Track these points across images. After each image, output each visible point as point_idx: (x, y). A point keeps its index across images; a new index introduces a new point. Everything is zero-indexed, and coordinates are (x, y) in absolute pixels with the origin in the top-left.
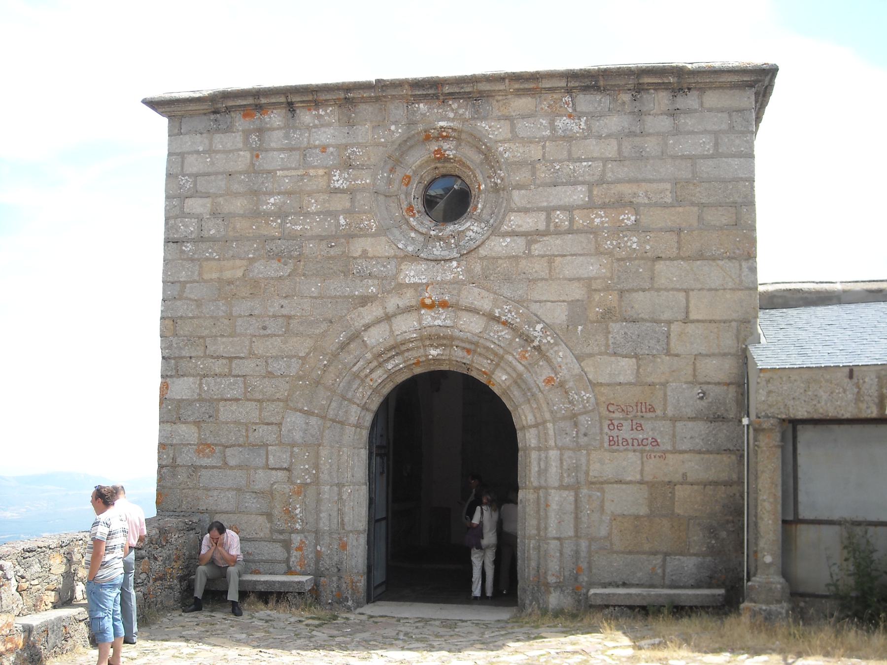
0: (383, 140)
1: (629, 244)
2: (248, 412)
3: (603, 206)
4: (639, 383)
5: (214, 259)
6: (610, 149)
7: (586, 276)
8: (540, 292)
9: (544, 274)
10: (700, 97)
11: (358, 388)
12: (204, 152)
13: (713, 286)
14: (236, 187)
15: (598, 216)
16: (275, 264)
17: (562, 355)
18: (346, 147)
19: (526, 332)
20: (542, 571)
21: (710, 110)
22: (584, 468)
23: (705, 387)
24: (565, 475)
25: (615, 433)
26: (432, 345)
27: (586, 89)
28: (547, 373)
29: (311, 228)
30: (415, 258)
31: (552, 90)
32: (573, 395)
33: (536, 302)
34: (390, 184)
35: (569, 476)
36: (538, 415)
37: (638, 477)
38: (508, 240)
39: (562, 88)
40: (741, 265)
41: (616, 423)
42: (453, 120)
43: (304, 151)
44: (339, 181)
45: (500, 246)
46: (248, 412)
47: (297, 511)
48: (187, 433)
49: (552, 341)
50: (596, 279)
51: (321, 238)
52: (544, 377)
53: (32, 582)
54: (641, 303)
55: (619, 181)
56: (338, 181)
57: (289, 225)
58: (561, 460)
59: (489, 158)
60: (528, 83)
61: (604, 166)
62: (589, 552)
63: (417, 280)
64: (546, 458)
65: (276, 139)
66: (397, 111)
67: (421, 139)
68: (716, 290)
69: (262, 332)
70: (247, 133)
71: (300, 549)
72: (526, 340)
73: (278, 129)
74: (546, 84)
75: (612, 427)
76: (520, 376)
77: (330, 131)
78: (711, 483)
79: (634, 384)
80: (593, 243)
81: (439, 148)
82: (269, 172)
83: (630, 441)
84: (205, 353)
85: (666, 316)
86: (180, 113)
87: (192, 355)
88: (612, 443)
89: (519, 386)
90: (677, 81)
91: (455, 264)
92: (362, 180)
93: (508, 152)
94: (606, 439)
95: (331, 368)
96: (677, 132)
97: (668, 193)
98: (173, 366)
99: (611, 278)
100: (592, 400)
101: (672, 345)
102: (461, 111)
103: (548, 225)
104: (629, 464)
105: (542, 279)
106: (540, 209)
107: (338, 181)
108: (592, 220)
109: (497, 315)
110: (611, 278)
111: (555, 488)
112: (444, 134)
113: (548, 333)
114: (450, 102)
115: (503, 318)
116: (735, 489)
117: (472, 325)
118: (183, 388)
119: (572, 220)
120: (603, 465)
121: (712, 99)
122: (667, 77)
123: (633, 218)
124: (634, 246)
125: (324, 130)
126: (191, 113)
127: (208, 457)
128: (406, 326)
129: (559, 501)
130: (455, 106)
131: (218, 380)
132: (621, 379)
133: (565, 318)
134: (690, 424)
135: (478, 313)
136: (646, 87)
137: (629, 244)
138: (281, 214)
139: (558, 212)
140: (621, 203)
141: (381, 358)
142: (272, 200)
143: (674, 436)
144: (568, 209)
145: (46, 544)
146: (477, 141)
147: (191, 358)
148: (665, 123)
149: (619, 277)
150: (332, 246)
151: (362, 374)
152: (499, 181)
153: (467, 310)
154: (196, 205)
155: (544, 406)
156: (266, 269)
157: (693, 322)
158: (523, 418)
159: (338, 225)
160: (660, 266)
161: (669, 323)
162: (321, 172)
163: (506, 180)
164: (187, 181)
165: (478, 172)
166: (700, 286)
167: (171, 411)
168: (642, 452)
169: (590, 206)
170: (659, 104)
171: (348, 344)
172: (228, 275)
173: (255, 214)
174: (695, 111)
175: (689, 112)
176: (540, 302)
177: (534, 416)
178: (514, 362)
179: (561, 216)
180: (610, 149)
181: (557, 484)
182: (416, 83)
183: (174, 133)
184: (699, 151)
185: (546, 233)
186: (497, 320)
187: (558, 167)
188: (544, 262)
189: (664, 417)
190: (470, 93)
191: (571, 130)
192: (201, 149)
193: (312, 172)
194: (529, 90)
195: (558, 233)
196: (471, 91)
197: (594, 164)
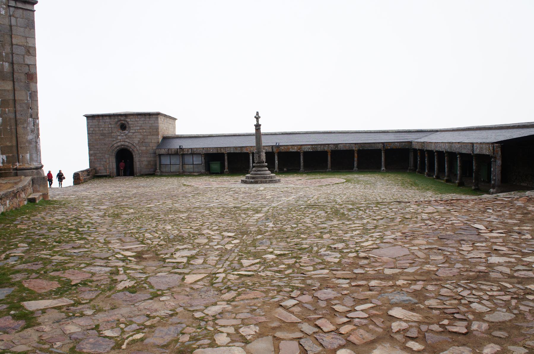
2: (100, 155)
6: (142, 122)
8: (135, 139)
17: (137, 147)
43: (105, 122)
44: (110, 126)
45: (130, 134)
46: (100, 155)
48: (92, 158)
54: (146, 141)
59: (128, 123)
65: (101, 121)
66: (116, 117)
81: (122, 121)
90: (150, 115)
93: (130, 123)
98: (90, 150)
104: (145, 159)
117: (127, 144)
118: (92, 152)
120: (143, 159)
121: (154, 116)
128: (119, 144)
129: (138, 163)
138: (103, 130)
140: (143, 129)
141: (116, 148)
146: (126, 121)
148: (148, 119)
154: (91, 129)
156: (101, 137)
167: (90, 155)
173: (99, 130)
180: (142, 122)
183: (87, 120)
196: (126, 115)
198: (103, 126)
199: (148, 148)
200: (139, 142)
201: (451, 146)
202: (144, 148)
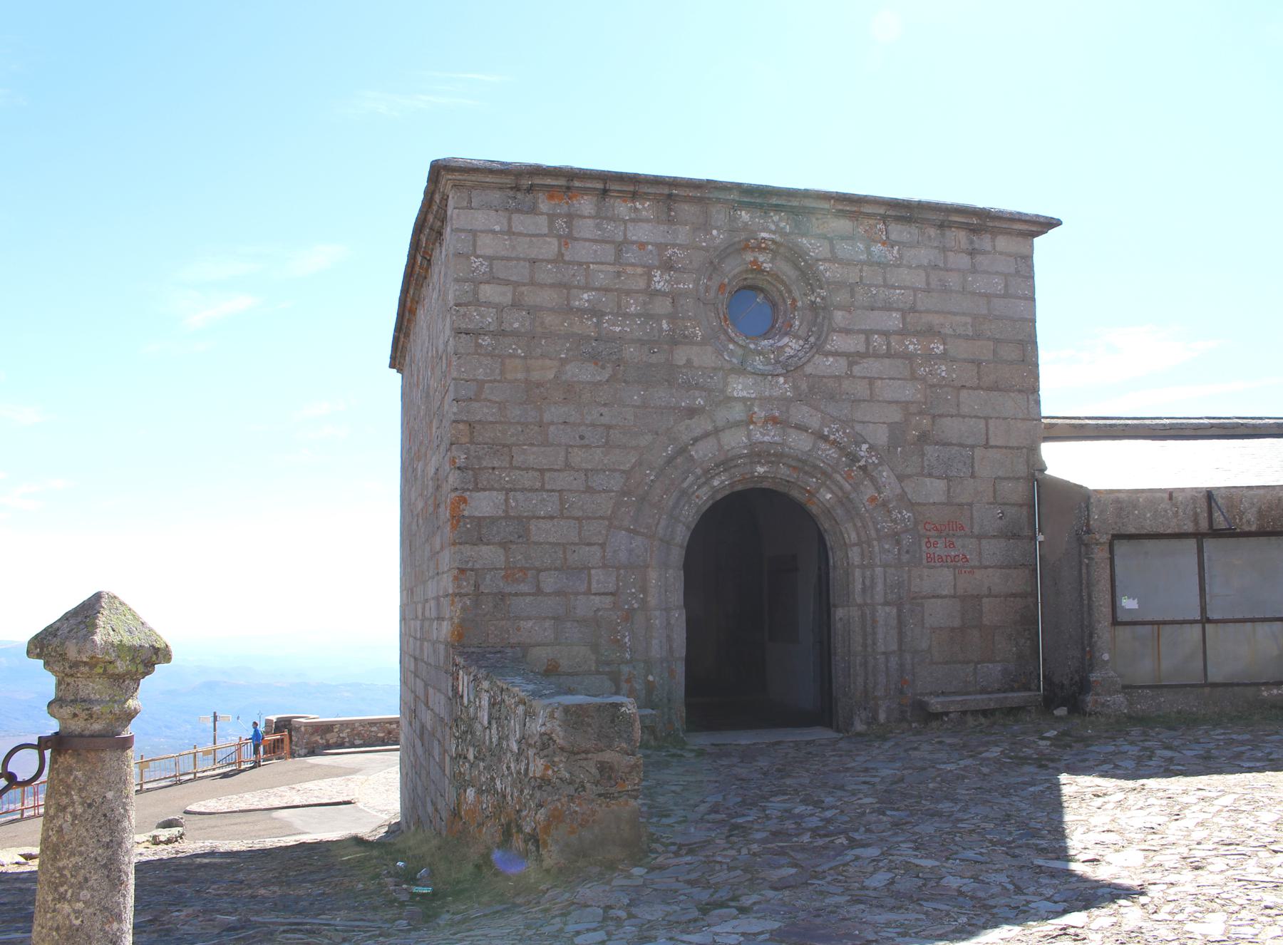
3: (917, 333)
10: (993, 240)
12: (501, 232)
25: (932, 550)
26: (759, 462)
28: (870, 492)
31: (869, 215)
32: (895, 514)
38: (831, 359)
41: (932, 540)
42: (774, 233)
44: (660, 281)
51: (641, 342)
55: (928, 311)
63: (745, 394)
65: (586, 228)
70: (552, 218)
85: (970, 441)
89: (843, 504)
91: (781, 380)
96: (974, 270)
99: (925, 403)
103: (867, 348)
110: (925, 403)
115: (832, 437)
119: (889, 345)
130: (776, 218)
133: (886, 439)
142: (585, 296)
144: (885, 334)
148: (965, 261)
156: (582, 373)
157: (992, 447)
159: (661, 330)
160: (964, 393)
161: (972, 447)
162: (639, 270)
165: (794, 288)
168: (955, 568)
169: (904, 333)
172: (536, 376)
174: (989, 253)
175: (984, 253)
177: (858, 534)
178: (842, 482)
185: (865, 355)
186: (825, 438)
192: (497, 228)
193: (629, 270)
195: (876, 355)
198: (602, 277)
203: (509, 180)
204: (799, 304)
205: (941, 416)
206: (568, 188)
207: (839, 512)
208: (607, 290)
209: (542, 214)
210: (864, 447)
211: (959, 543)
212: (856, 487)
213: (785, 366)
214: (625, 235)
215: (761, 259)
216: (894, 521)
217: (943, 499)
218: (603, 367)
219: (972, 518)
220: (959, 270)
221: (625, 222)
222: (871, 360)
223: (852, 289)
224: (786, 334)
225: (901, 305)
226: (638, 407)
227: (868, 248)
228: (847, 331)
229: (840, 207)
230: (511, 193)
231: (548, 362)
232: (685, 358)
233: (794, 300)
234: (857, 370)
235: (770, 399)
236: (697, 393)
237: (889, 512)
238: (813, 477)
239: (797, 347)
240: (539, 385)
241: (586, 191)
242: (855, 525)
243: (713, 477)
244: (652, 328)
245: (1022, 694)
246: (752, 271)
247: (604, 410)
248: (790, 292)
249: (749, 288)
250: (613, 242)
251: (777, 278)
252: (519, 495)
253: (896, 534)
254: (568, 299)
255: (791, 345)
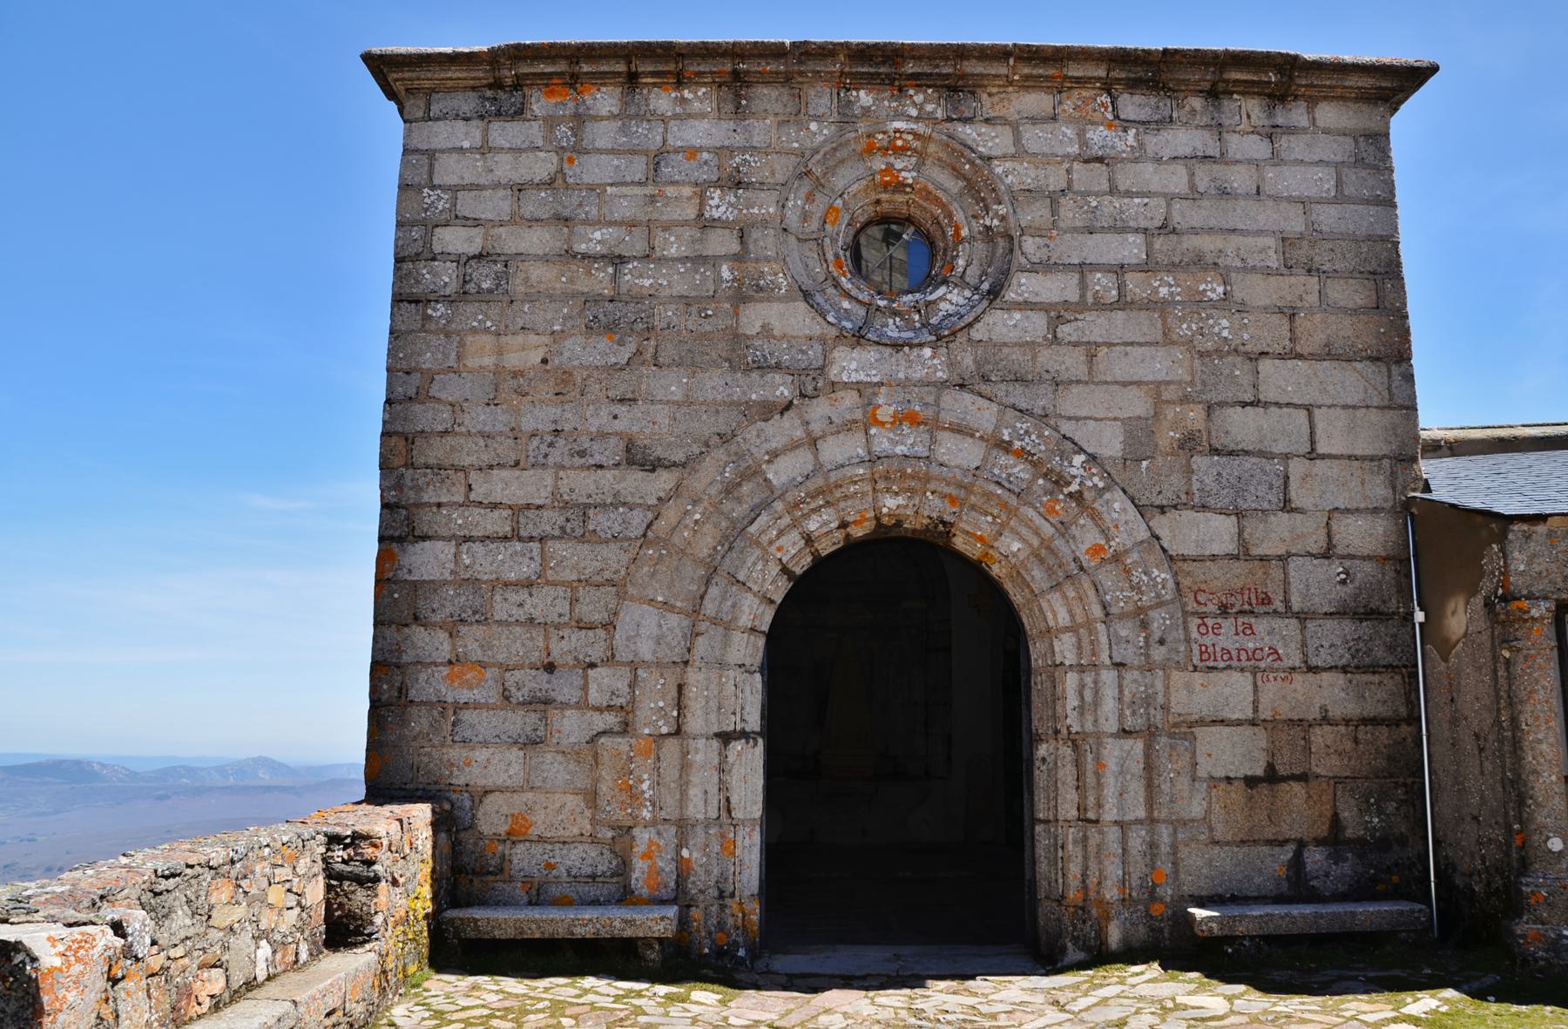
0: (796, 145)
1: (1216, 329)
3: (1173, 267)
4: (1243, 553)
5: (487, 330)
7: (1151, 378)
8: (1073, 402)
9: (1081, 371)
10: (1310, 110)
11: (755, 564)
12: (471, 150)
13: (1349, 402)
14: (529, 209)
15: (1163, 283)
16: (603, 343)
18: (731, 150)
19: (1058, 469)
20: (1093, 880)
21: (1327, 131)
22: (1160, 699)
23: (1347, 563)
24: (1128, 712)
25: (1208, 640)
26: (888, 490)
27: (1133, 85)
28: (1091, 537)
29: (670, 285)
30: (858, 338)
31: (1081, 82)
32: (1138, 575)
33: (1069, 418)
34: (805, 220)
35: (1134, 713)
36: (1078, 611)
37: (1250, 714)
38: (1017, 316)
39: (1099, 79)
40: (1389, 371)
41: (1210, 622)
42: (917, 119)
44: (719, 205)
47: (645, 786)
49: (1101, 485)
50: (1168, 383)
51: (686, 301)
52: (1087, 546)
53: (173, 953)
55: (1194, 231)
56: (718, 207)
57: (628, 277)
58: (1120, 686)
59: (979, 186)
60: (1046, 65)
61: (1169, 205)
62: (1174, 848)
63: (862, 377)
64: (1096, 682)
65: (603, 134)
67: (859, 149)
68: (1354, 407)
69: (578, 461)
70: (551, 122)
71: (647, 856)
72: (1056, 482)
73: (608, 118)
74: (1075, 70)
75: (1203, 630)
76: (1047, 544)
77: (704, 125)
78: (1365, 721)
79: (1237, 558)
80: (1159, 326)
82: (591, 188)
83: (1234, 654)
84: (467, 497)
85: (1280, 448)
86: (427, 84)
87: (444, 500)
88: (1205, 656)
89: (1042, 561)
90: (1282, 79)
91: (927, 352)
92: (761, 207)
93: (1011, 174)
94: (1196, 648)
95: (708, 527)
96: (1276, 159)
97: (1271, 253)
99: (1192, 383)
100: (1171, 584)
101: (1293, 495)
102: (929, 108)
103: (1083, 296)
105: (1078, 382)
106: (1068, 267)
107: (718, 207)
108: (1156, 291)
109: (1006, 438)
110: (1192, 383)
111: (1112, 735)
112: (899, 143)
113: (1094, 471)
114: (911, 92)
115: (1017, 444)
116: (1405, 729)
119: (1121, 288)
120: (1193, 694)
122: (1266, 73)
123: (1220, 289)
124: (1225, 333)
125: (695, 122)
126: (450, 83)
127: (471, 688)
130: (919, 98)
131: (492, 546)
132: (1217, 549)
133: (1119, 447)
134: (1330, 624)
135: (972, 436)
136: (1230, 87)
137: (1216, 329)
139: (1099, 275)
140: (1199, 263)
142: (598, 235)
143: (1304, 644)
144: (1120, 269)
145: (203, 860)
146: (960, 158)
147: (439, 505)
148: (1257, 147)
149: (1204, 383)
150: (707, 316)
151: (764, 539)
152: (996, 222)
153: (953, 430)
155: (1091, 593)
156: (584, 352)
157: (1323, 457)
158: (1049, 615)
159: (718, 279)
160: (1266, 365)
161: (1286, 457)
162: (687, 191)
163: (1011, 219)
164: (439, 198)
165: (954, 207)
166: (1330, 402)
168: (1255, 671)
169: (1148, 267)
170: (1249, 117)
171: (740, 484)
172: (513, 360)
174: (1304, 130)
175: (1291, 130)
176: (1077, 419)
177: (1070, 612)
178: (1039, 521)
179: (1104, 281)
180: (1177, 180)
181: (1114, 729)
182: (862, 51)
184: (1313, 192)
185: (1081, 306)
186: (1006, 447)
187: (1094, 204)
188: (1079, 355)
189: (1288, 612)
190: (947, 76)
191: (1113, 147)
192: (466, 145)
193: (670, 191)
194: (1047, 78)
195: (1100, 306)
197: (1153, 202)
198: (626, 205)
199: (1274, 535)
200: (1139, 439)
201: (955, 109)
202: (1217, 533)
203: (481, 73)
204: (964, 232)
205: (1222, 404)
206: (573, 76)
207: (1037, 576)
208: (632, 224)
209: (536, 118)
210: (1079, 459)
211: (1261, 626)
212: (1063, 528)
213: (935, 330)
214: (665, 141)
215: (899, 165)
216: (1136, 588)
217: (1232, 548)
218: (621, 343)
219: (1286, 582)
220: (1250, 162)
221: (664, 120)
222: (1089, 316)
223: (1054, 200)
224: (945, 282)
225: (1143, 224)
226: (678, 404)
227: (1081, 134)
228: (1045, 267)
229: (1026, 71)
230: (489, 93)
231: (533, 338)
232: (758, 324)
233: (957, 229)
234: (1064, 330)
235: (905, 384)
236: (778, 378)
237: (1127, 571)
238: (986, 514)
239: (961, 301)
240: (516, 374)
241: (601, 78)
242: (1065, 597)
243: (806, 516)
244: (704, 279)
245: (1386, 907)
246: (885, 187)
247: (622, 409)
248: (950, 216)
249: (888, 224)
250: (646, 153)
251: (928, 195)
252: (477, 547)
253: (1140, 610)
254: (569, 240)
255: (950, 300)
